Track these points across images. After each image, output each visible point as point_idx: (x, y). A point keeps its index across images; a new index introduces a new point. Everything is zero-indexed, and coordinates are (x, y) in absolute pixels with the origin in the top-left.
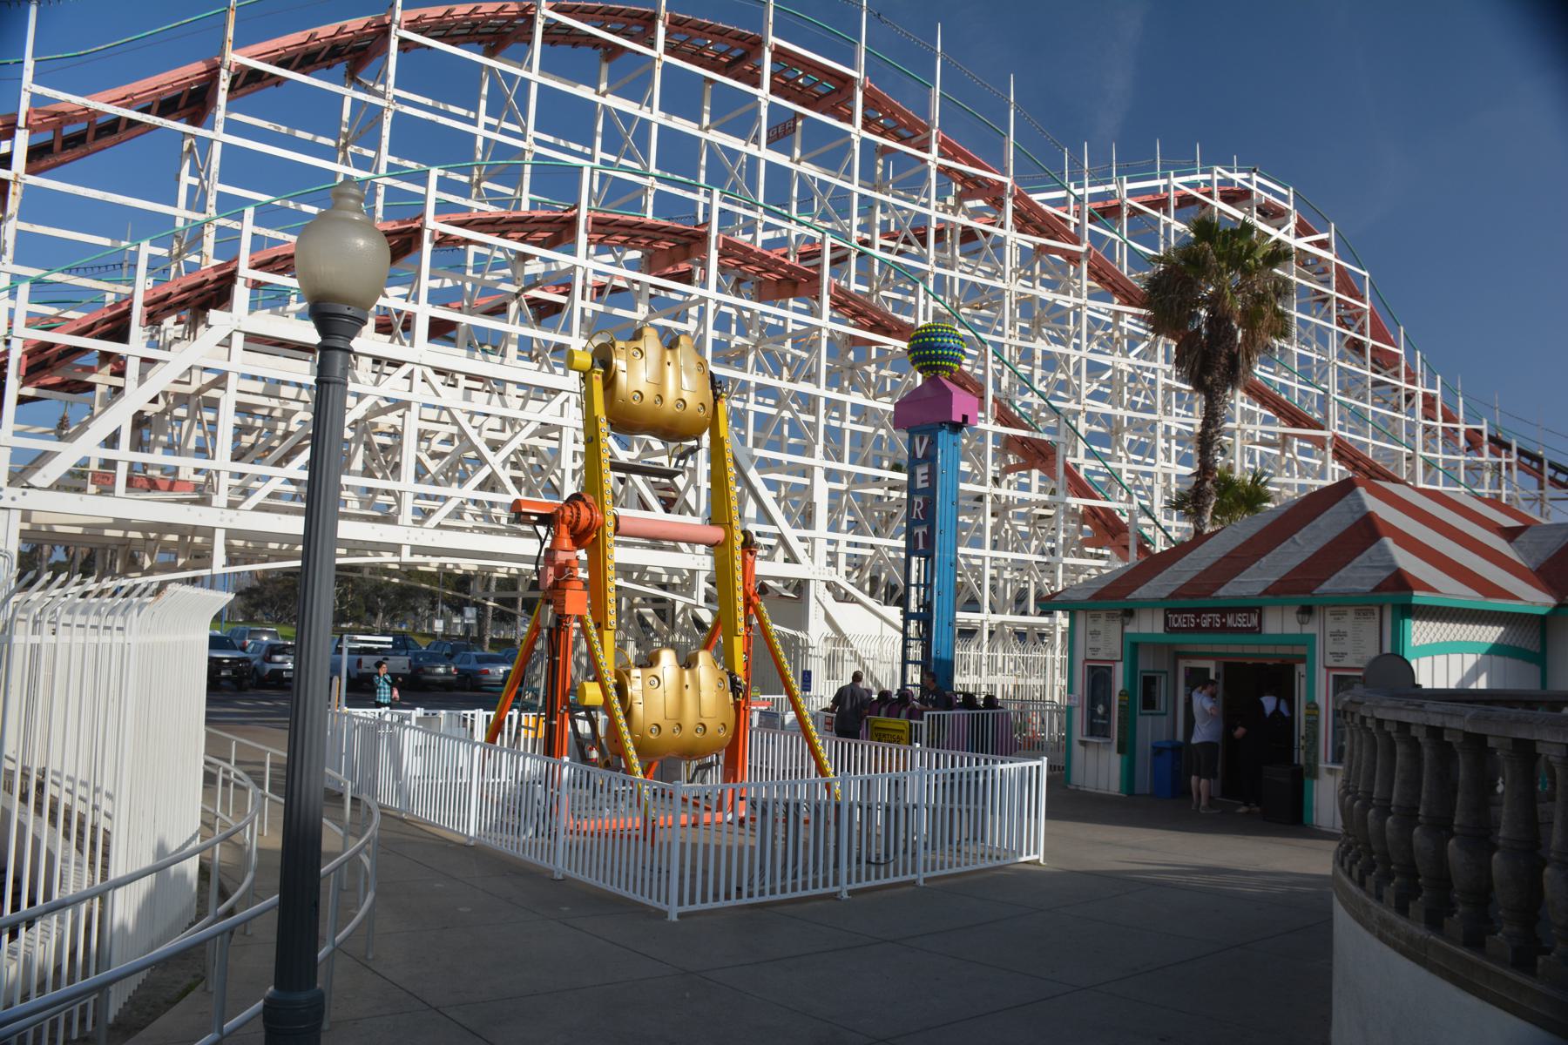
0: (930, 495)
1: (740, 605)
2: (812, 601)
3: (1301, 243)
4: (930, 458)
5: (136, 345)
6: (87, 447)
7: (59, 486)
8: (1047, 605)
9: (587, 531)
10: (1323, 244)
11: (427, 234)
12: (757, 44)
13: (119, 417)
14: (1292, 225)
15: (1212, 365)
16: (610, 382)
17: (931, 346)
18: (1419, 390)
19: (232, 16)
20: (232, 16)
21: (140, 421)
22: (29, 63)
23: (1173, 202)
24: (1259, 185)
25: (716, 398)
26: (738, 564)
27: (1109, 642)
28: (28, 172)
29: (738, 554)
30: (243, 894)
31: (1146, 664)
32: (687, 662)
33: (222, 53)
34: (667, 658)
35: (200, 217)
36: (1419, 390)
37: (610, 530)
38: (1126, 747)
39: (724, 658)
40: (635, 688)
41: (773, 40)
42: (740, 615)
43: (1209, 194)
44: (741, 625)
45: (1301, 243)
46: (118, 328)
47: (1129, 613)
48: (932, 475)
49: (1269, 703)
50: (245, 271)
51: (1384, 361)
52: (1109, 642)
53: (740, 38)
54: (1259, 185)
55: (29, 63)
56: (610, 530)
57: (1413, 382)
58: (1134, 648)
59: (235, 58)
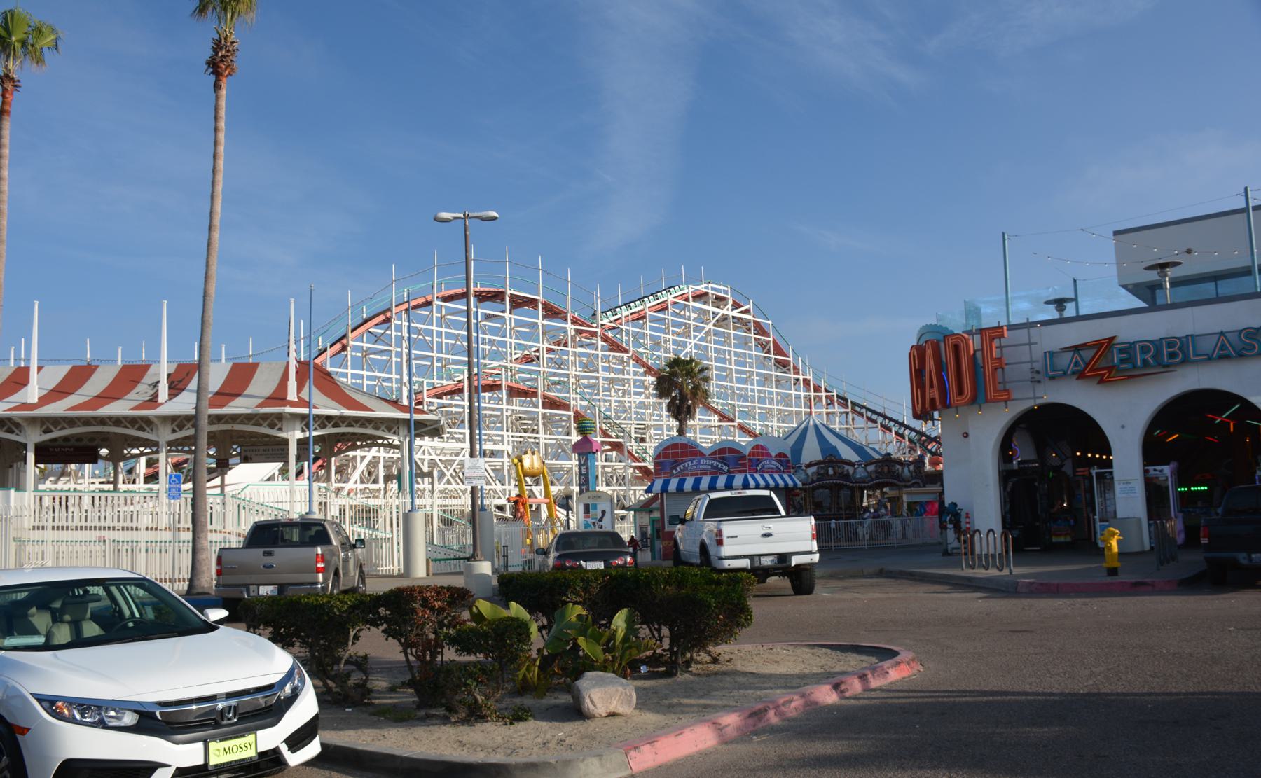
0: (587, 476)
3: (735, 313)
4: (586, 463)
8: (628, 509)
10: (747, 311)
12: (503, 293)
14: (730, 306)
15: (681, 411)
18: (801, 377)
24: (713, 289)
27: (645, 519)
30: (41, 716)
31: (656, 526)
36: (801, 377)
38: (652, 551)
41: (509, 292)
43: (687, 300)
45: (735, 313)
47: (651, 512)
48: (587, 469)
49: (104, 452)
51: (783, 365)
52: (645, 519)
54: (713, 289)
57: (797, 373)
58: (653, 521)
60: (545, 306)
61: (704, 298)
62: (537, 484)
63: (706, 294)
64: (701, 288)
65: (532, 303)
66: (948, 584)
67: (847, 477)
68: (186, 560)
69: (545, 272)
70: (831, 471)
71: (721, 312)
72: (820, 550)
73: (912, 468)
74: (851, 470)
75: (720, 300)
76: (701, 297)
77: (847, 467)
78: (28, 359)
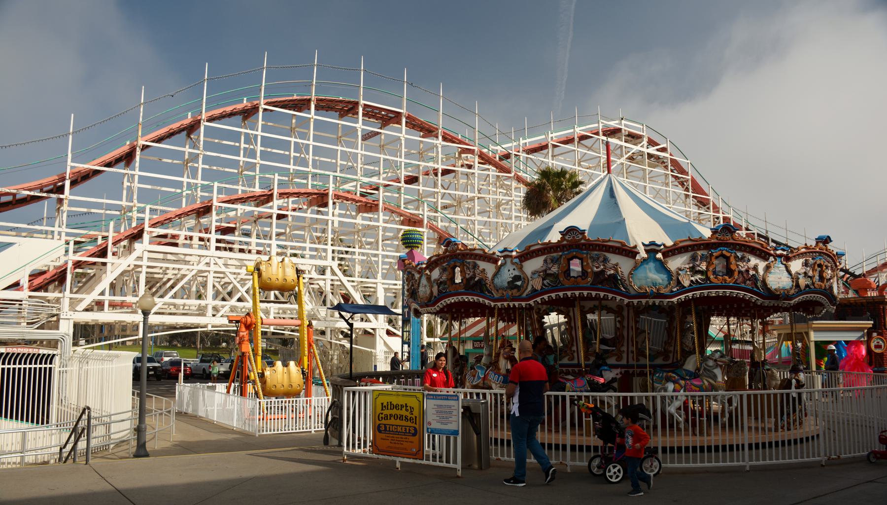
1: (306, 346)
2: (378, 337)
5: (110, 258)
6: (94, 296)
7: (86, 310)
9: (250, 325)
10: (664, 150)
11: (214, 207)
12: (356, 104)
13: (105, 284)
14: (645, 142)
16: (260, 275)
17: (410, 239)
19: (140, 127)
20: (140, 127)
21: (112, 286)
22: (70, 155)
23: (576, 139)
25: (298, 277)
26: (306, 332)
28: (70, 194)
29: (306, 329)
32: (286, 365)
33: (137, 140)
34: (279, 364)
35: (131, 204)
37: (259, 324)
39: (299, 363)
40: (267, 373)
41: (362, 102)
42: (306, 349)
44: (306, 352)
45: (652, 150)
46: (103, 253)
50: (147, 228)
53: (349, 102)
54: (626, 125)
55: (70, 155)
56: (259, 324)
59: (141, 142)
60: (408, 117)
61: (618, 135)
62: (749, 260)
63: (619, 130)
64: (614, 124)
65: (396, 117)
66: (497, 168)
67: (613, 282)
68: (349, 369)
69: (410, 84)
70: (576, 267)
71: (636, 148)
72: (753, 318)
73: (796, 266)
74: (489, 269)
75: (634, 138)
76: (613, 132)
77: (614, 259)
78: (393, 257)
